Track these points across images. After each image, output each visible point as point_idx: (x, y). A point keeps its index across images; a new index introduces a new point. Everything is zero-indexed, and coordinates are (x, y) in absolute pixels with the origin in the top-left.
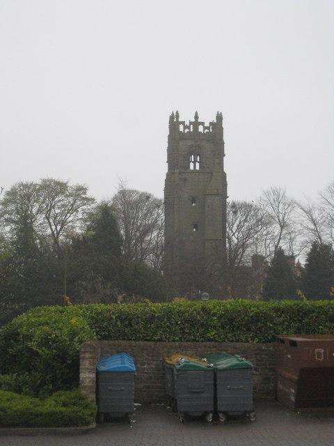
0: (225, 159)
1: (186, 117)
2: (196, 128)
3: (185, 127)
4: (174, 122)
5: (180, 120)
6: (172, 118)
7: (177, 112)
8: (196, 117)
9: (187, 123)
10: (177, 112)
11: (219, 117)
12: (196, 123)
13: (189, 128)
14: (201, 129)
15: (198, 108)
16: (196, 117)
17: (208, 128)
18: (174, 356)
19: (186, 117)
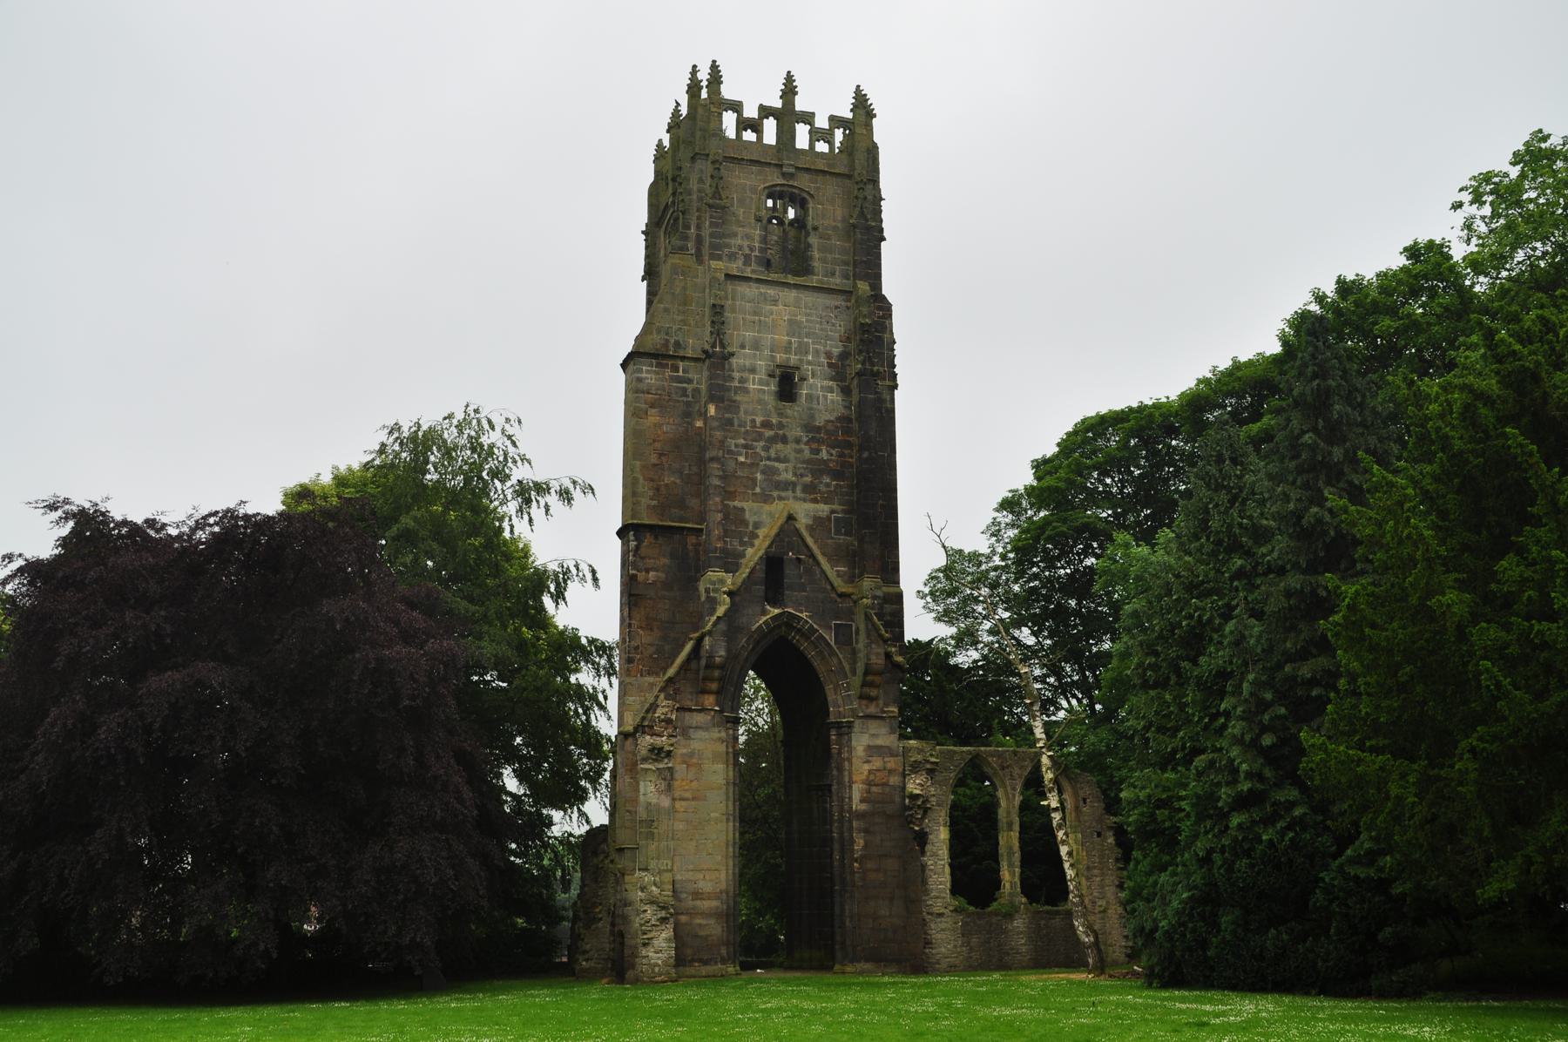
1: (751, 89)
2: (786, 134)
8: (789, 91)
10: (714, 67)
11: (861, 104)
12: (787, 115)
16: (789, 91)
19: (751, 89)
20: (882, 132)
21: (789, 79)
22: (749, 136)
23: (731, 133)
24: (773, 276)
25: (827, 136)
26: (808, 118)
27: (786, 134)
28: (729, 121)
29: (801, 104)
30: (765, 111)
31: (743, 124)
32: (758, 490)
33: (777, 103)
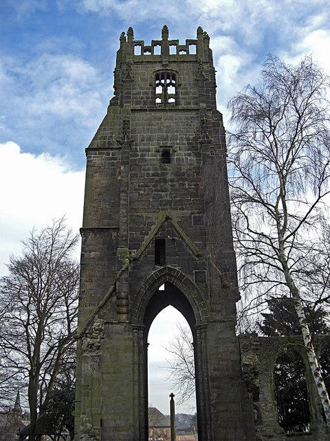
2: (165, 51)
8: (165, 31)
12: (165, 44)
16: (165, 31)
22: (148, 53)
27: (165, 51)
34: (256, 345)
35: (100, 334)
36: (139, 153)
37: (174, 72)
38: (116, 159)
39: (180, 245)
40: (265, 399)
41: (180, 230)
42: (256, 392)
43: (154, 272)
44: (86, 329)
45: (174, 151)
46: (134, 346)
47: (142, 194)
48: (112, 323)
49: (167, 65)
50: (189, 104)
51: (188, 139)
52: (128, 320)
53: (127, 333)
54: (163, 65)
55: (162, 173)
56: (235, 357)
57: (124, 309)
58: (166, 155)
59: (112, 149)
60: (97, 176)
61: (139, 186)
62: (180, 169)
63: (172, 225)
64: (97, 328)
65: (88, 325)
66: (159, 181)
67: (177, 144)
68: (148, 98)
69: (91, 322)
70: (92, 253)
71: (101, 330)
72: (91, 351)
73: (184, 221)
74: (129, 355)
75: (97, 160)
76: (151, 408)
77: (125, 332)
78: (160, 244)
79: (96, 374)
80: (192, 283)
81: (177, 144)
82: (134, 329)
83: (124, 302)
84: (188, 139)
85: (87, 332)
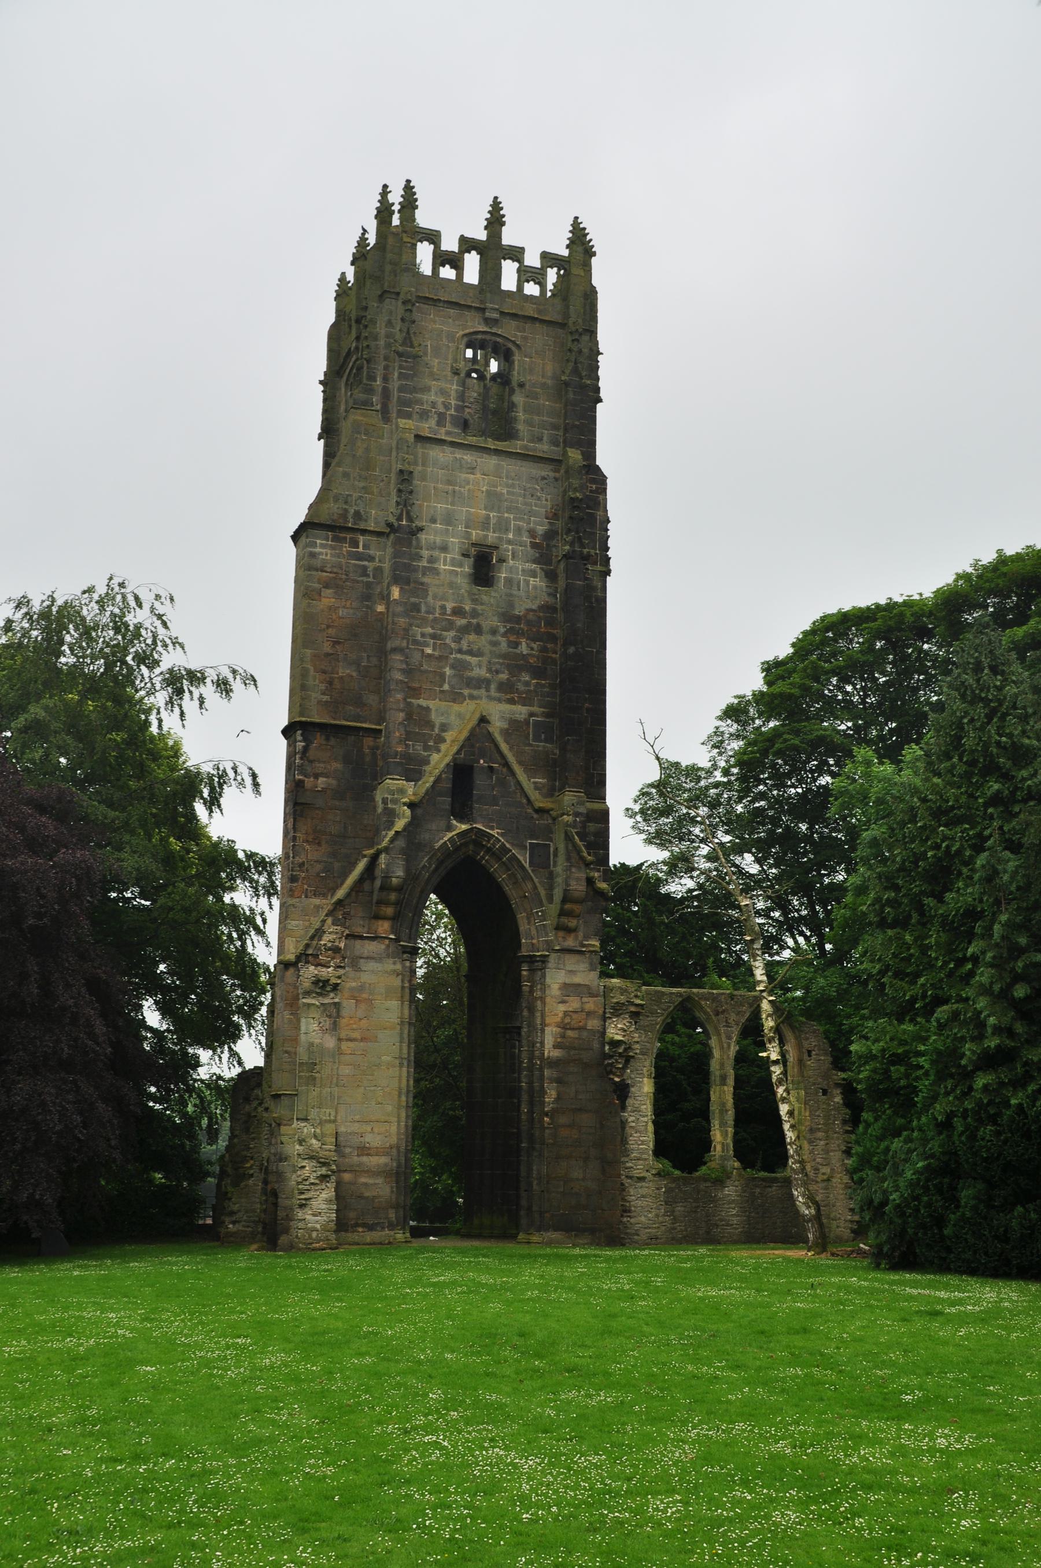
0: (601, 410)
1: (451, 216)
2: (490, 273)
3: (526, 274)
4: (397, 227)
5: (424, 219)
6: (260, 795)
7: (409, 189)
8: (496, 220)
9: (450, 244)
10: (409, 189)
11: (579, 238)
12: (493, 250)
13: (455, 261)
14: (509, 276)
15: (494, 180)
16: (496, 220)
17: (537, 276)
18: (376, 1145)
19: (451, 216)
20: (602, 274)
21: (496, 206)
22: (447, 273)
23: (426, 266)
24: (493, 338)
25: (537, 276)
26: (516, 254)
27: (490, 273)
28: (424, 253)
29: (509, 237)
30: (467, 244)
31: (441, 258)
32: (446, 687)
33: (482, 235)
34: (637, 1005)
35: (333, 958)
36: (425, 553)
37: (510, 345)
38: (371, 559)
39: (502, 783)
40: (637, 1110)
41: (504, 747)
42: (623, 1091)
43: (450, 835)
44: (307, 946)
45: (502, 560)
46: (403, 988)
47: (429, 655)
48: (361, 938)
49: (495, 322)
50: (540, 440)
51: (532, 533)
52: (392, 933)
53: (391, 961)
54: (487, 321)
55: (474, 610)
56: (594, 1024)
57: (390, 911)
58: (483, 566)
59: (364, 532)
60: (328, 599)
61: (423, 635)
62: (511, 605)
63: (490, 737)
64: (329, 945)
65: (312, 938)
66: (465, 630)
67: (509, 542)
68: (447, 406)
69: (319, 933)
70: (321, 780)
71: (336, 950)
72: (320, 994)
73: (515, 728)
74: (394, 1004)
75: (323, 548)
76: (769, 683)
77: (388, 956)
78: (461, 774)
79: (330, 1042)
80: (523, 867)
81: (509, 542)
82: (404, 952)
83: (393, 897)
84: (532, 533)
85: (310, 952)
